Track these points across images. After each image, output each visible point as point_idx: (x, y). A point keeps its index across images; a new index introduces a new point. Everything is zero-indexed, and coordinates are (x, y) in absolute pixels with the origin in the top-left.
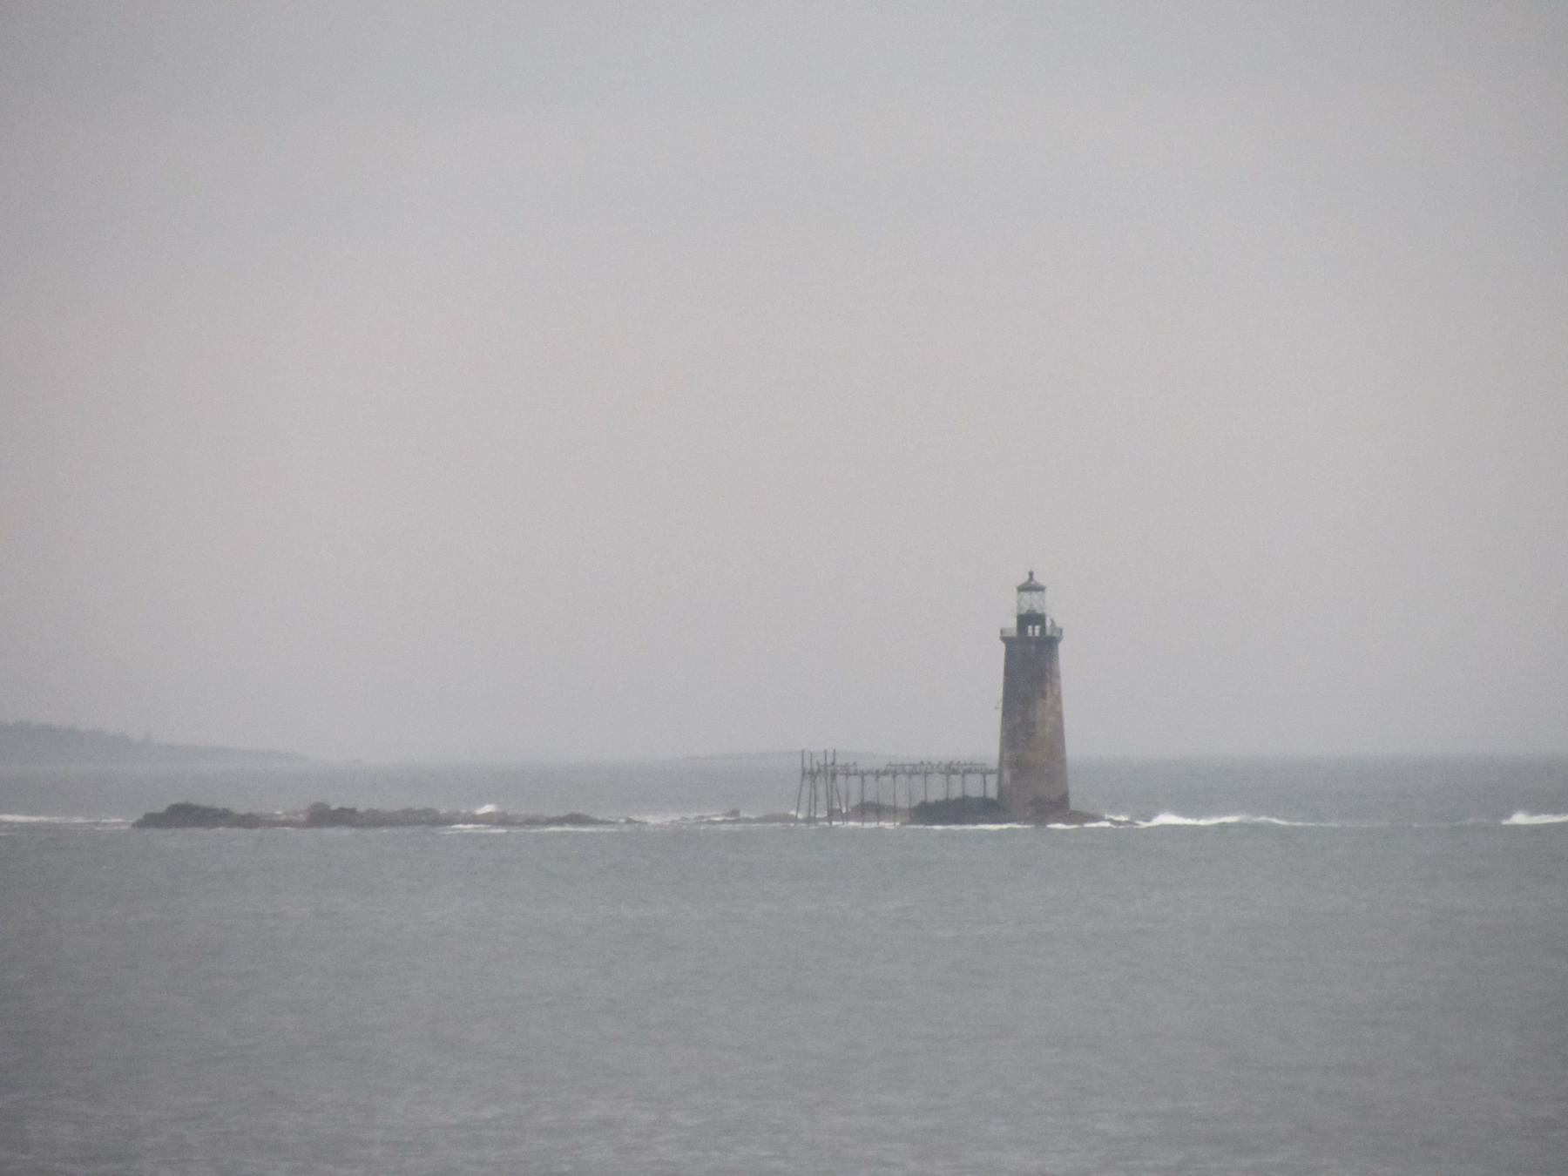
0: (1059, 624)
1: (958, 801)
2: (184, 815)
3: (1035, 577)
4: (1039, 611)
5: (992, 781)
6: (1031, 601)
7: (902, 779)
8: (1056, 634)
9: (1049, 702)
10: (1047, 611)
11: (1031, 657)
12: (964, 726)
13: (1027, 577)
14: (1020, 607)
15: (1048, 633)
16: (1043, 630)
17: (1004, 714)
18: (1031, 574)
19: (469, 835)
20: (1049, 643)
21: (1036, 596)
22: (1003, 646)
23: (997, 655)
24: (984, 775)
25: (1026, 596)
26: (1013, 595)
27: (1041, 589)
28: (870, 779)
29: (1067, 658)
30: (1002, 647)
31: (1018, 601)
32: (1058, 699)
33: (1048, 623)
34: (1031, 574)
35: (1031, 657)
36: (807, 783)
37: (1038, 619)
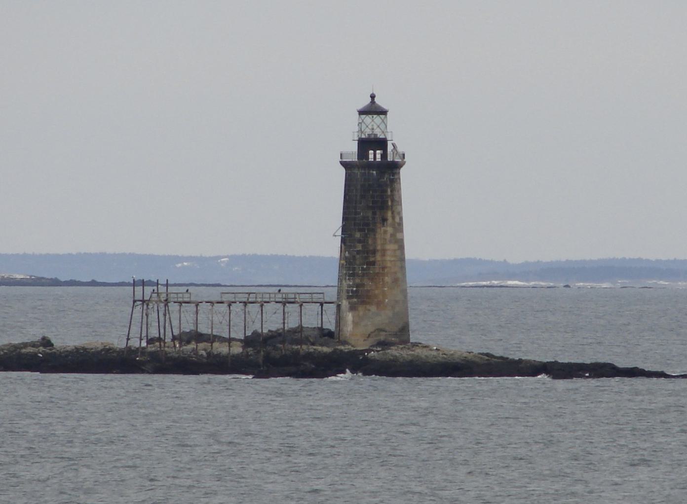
0: (400, 149)
1: (293, 331)
3: (376, 100)
6: (373, 126)
7: (237, 308)
8: (397, 159)
10: (389, 138)
11: (372, 185)
12: (298, 231)
13: (370, 100)
14: (361, 131)
15: (390, 159)
16: (384, 156)
17: (343, 241)
18: (373, 97)
19: (484, 281)
20: (391, 169)
21: (377, 119)
22: (342, 171)
23: (336, 182)
24: (229, 306)
25: (368, 119)
27: (384, 112)
28: (203, 307)
29: (411, 186)
32: (399, 227)
33: (390, 148)
34: (373, 97)
35: (372, 185)
36: (138, 309)
37: (381, 144)
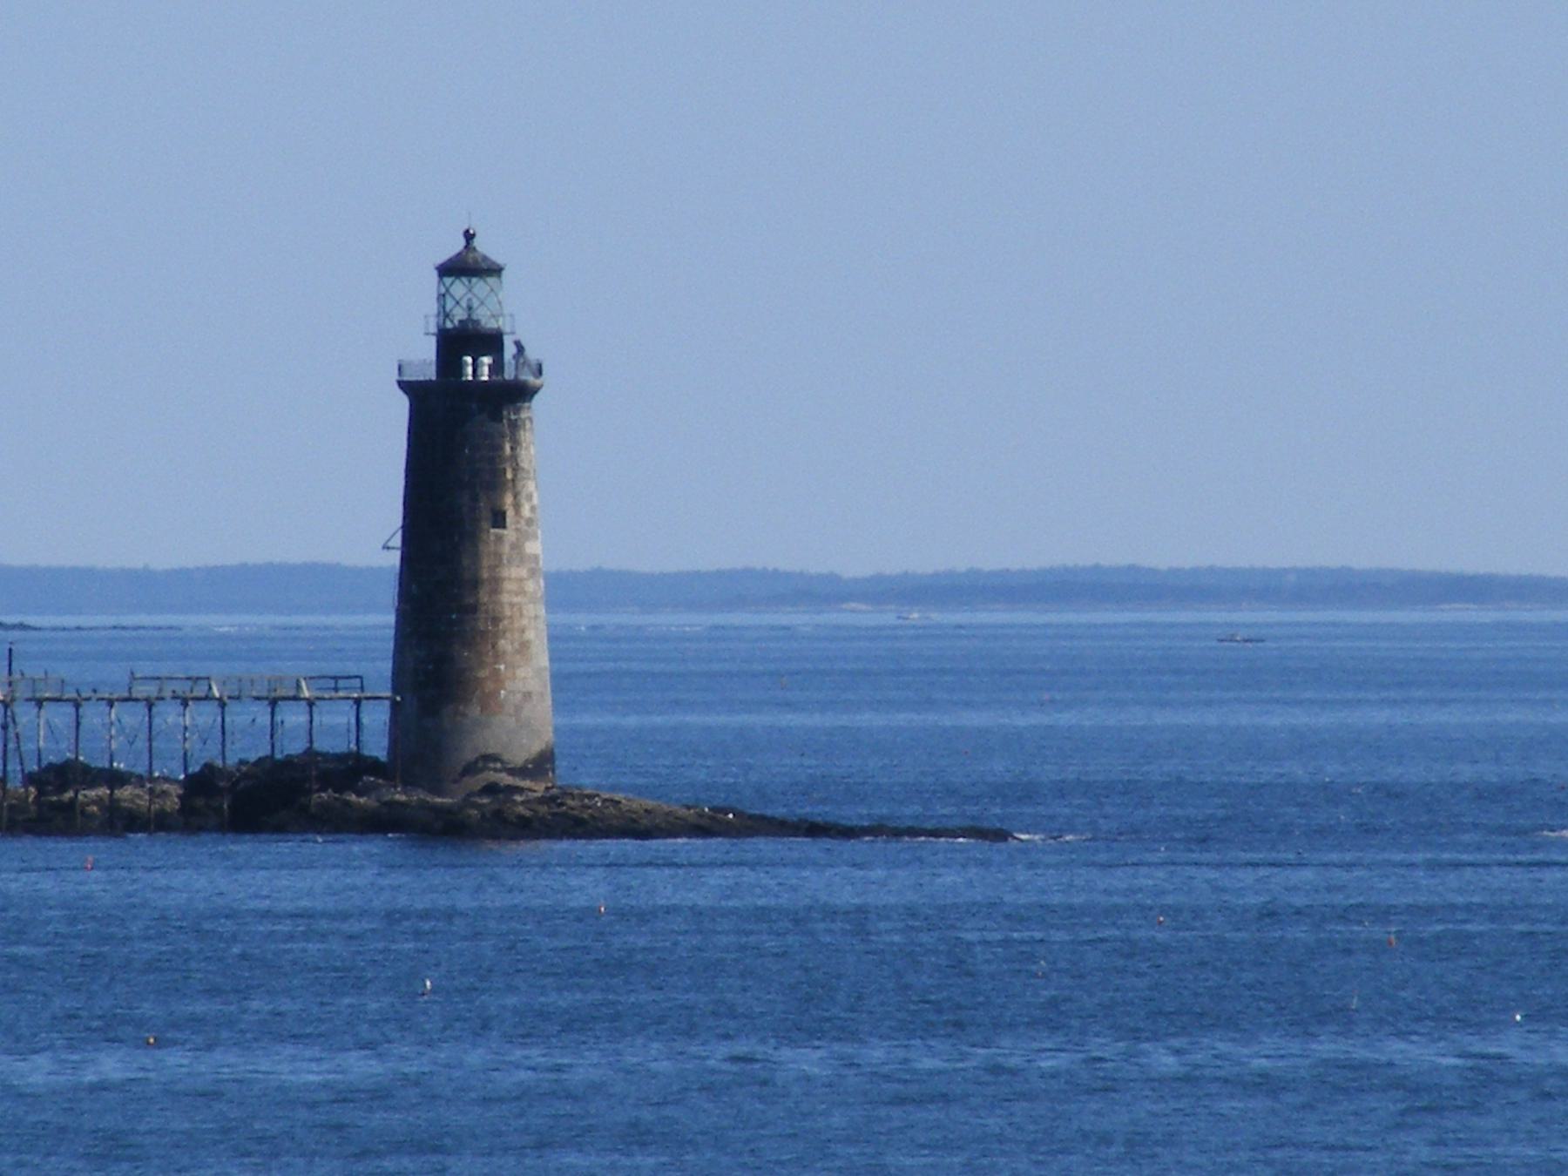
2: (1536, 780)
3: (476, 242)
4: (489, 324)
5: (377, 718)
9: (509, 534)
11: (462, 423)
13: (462, 242)
15: (509, 374)
16: (497, 367)
18: (469, 236)
21: (480, 286)
25: (459, 287)
26: (430, 281)
27: (495, 271)
30: (401, 405)
31: (442, 297)
33: (509, 350)
34: (469, 236)
35: (462, 423)
37: (491, 342)
